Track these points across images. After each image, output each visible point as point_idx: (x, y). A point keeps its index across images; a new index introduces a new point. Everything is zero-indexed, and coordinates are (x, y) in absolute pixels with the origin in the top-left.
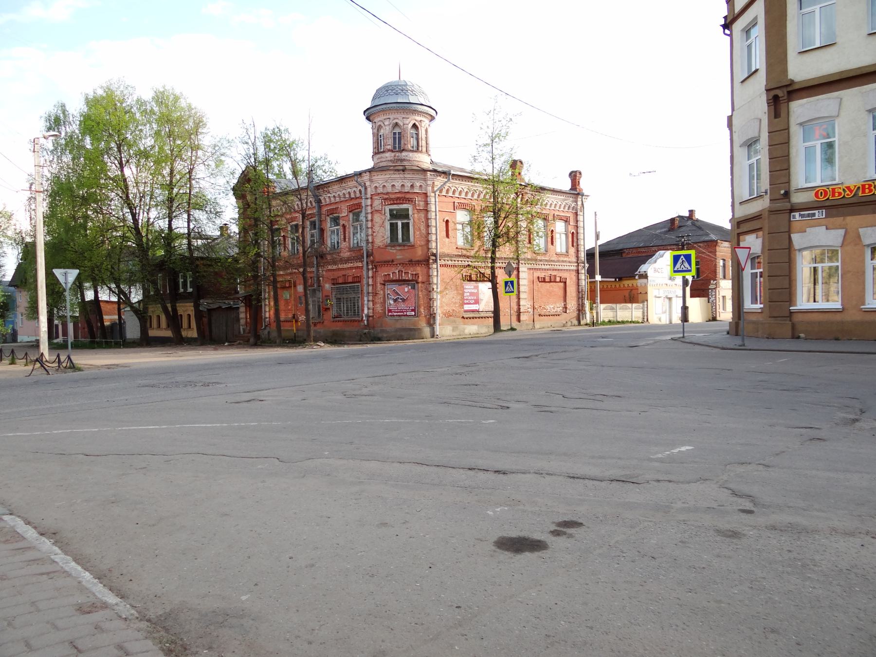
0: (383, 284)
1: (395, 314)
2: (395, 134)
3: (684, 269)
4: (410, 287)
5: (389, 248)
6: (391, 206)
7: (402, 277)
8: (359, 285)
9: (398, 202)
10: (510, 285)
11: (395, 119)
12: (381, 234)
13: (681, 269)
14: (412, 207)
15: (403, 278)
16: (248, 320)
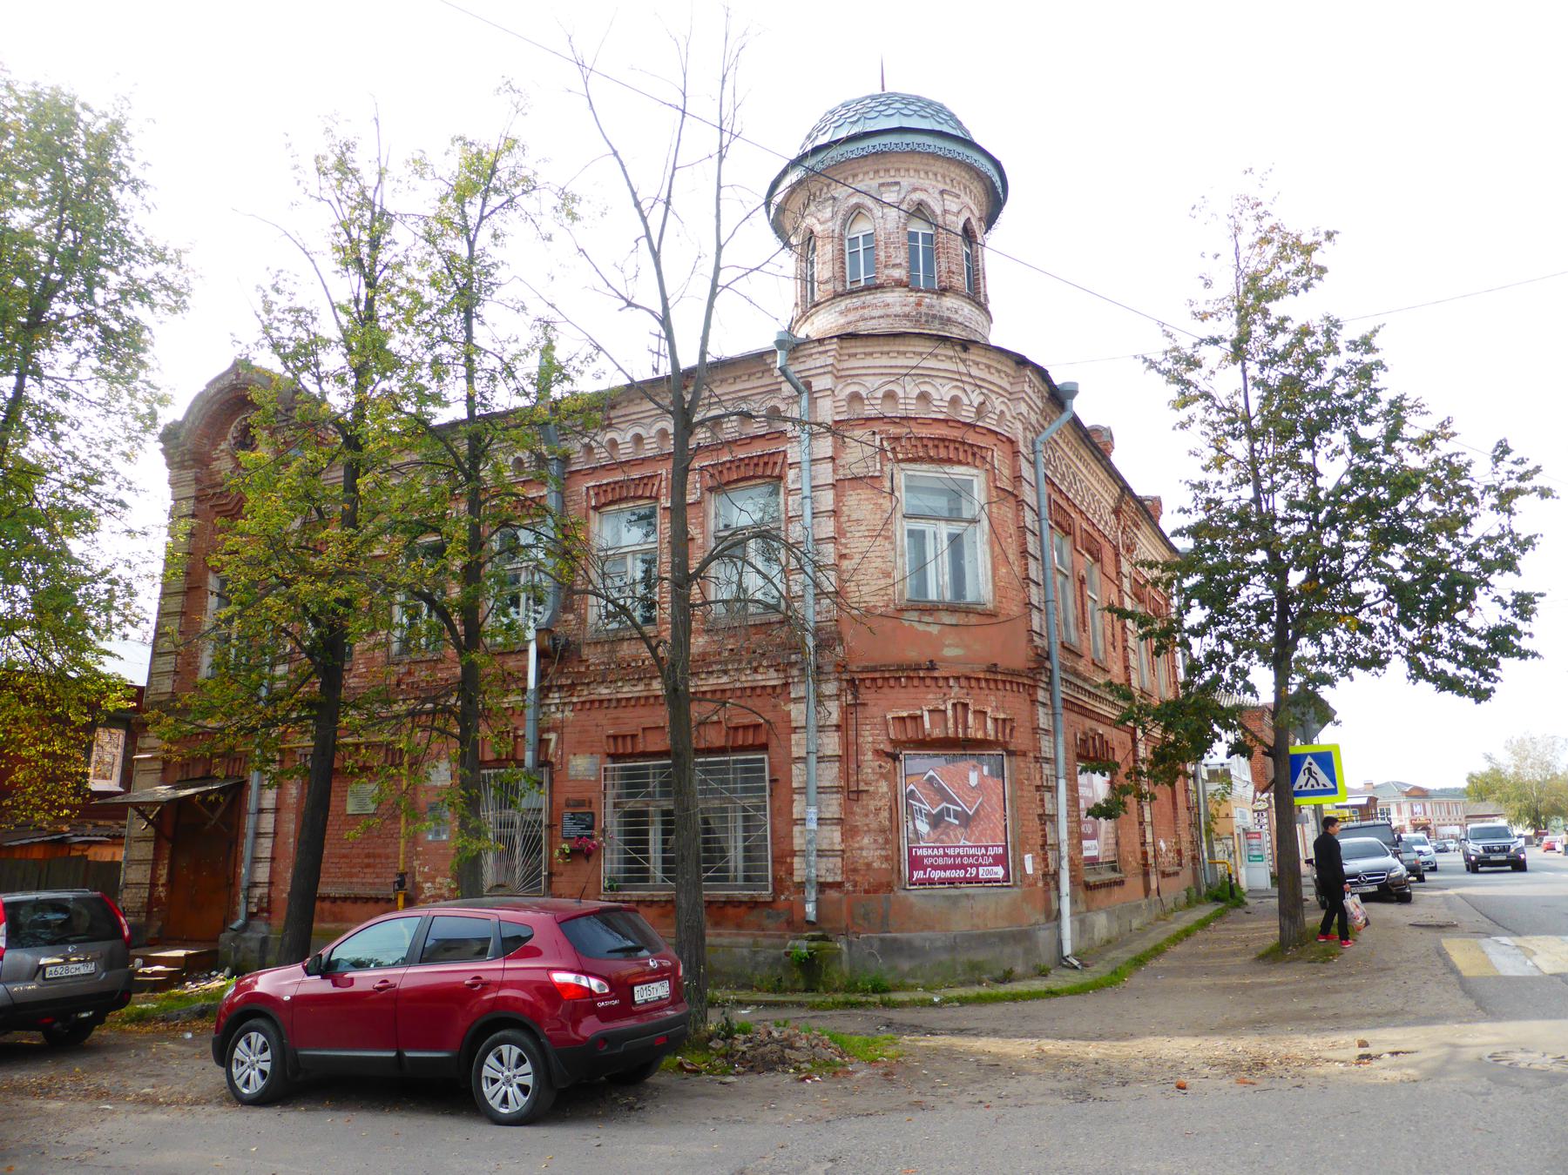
0: (888, 755)
1: (936, 875)
2: (913, 236)
3: (1316, 787)
4: (986, 770)
5: (914, 616)
6: (913, 466)
7: (966, 727)
8: (762, 760)
9: (943, 453)
10: (1315, 768)
11: (915, 190)
12: (878, 563)
13: (1309, 787)
15: (971, 733)
16: (161, 891)
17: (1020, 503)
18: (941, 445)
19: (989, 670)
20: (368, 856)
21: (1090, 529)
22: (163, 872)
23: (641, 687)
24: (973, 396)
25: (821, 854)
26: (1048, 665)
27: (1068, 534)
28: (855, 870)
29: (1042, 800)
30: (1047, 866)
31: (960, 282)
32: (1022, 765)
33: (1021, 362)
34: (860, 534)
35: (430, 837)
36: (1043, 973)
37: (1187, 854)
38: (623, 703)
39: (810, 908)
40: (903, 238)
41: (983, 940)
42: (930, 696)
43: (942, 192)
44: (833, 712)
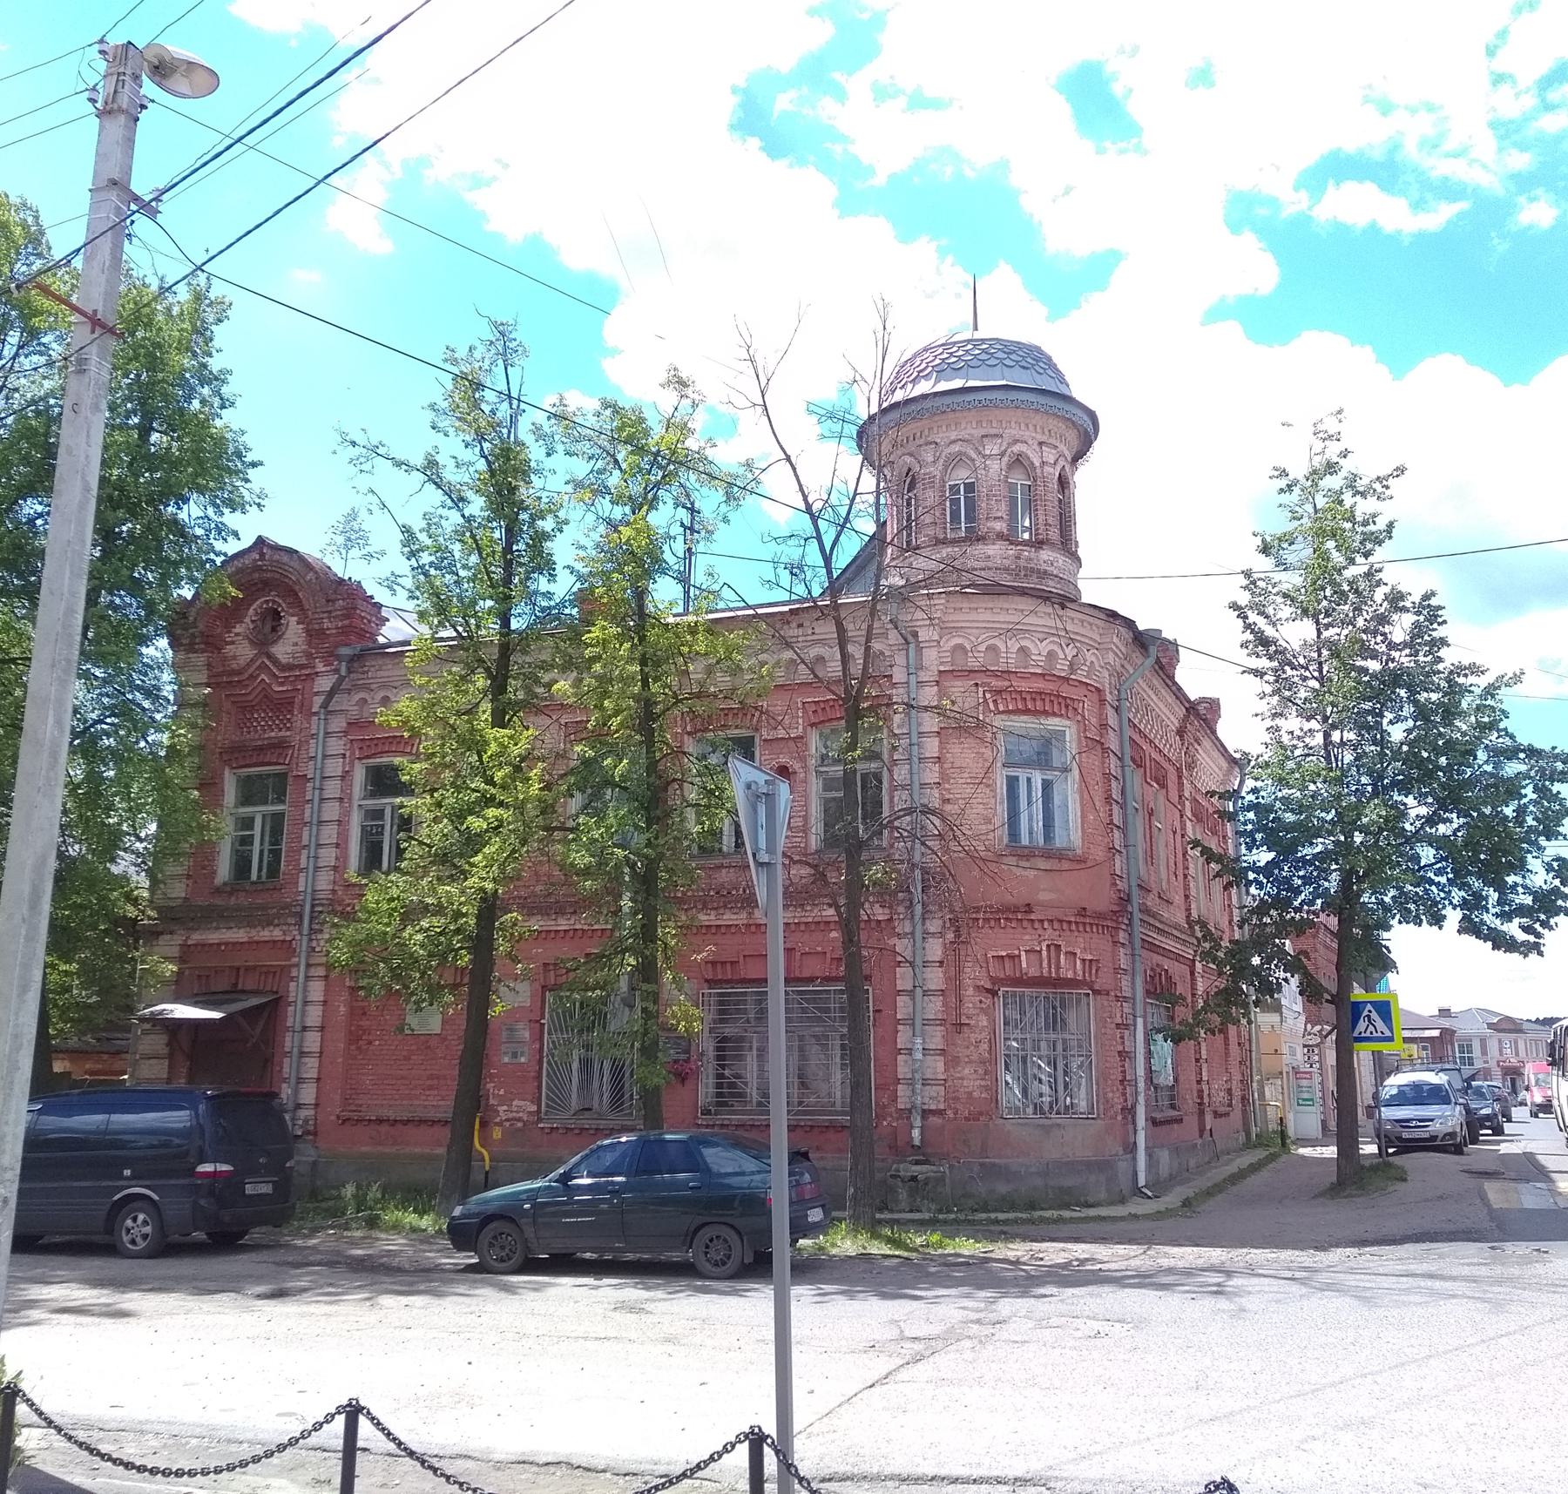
0: (988, 991)
3: (1375, 1034)
7: (1058, 967)
10: (1374, 1015)
11: (1016, 441)
13: (1368, 1034)
14: (1074, 729)
17: (1105, 750)
18: (1038, 697)
19: (1079, 914)
20: (431, 1077)
21: (1158, 758)
23: (744, 915)
24: (1067, 651)
25: (926, 1082)
26: (1130, 909)
27: (1139, 766)
28: (956, 1099)
29: (1122, 1038)
30: (1126, 1101)
31: (1054, 534)
32: (1106, 1003)
33: (1113, 615)
34: (963, 781)
35: (506, 1060)
36: (1122, 1201)
37: (1237, 1093)
38: (723, 930)
39: (916, 1133)
41: (1071, 1166)
42: (1027, 937)
43: (1041, 444)
44: (935, 949)
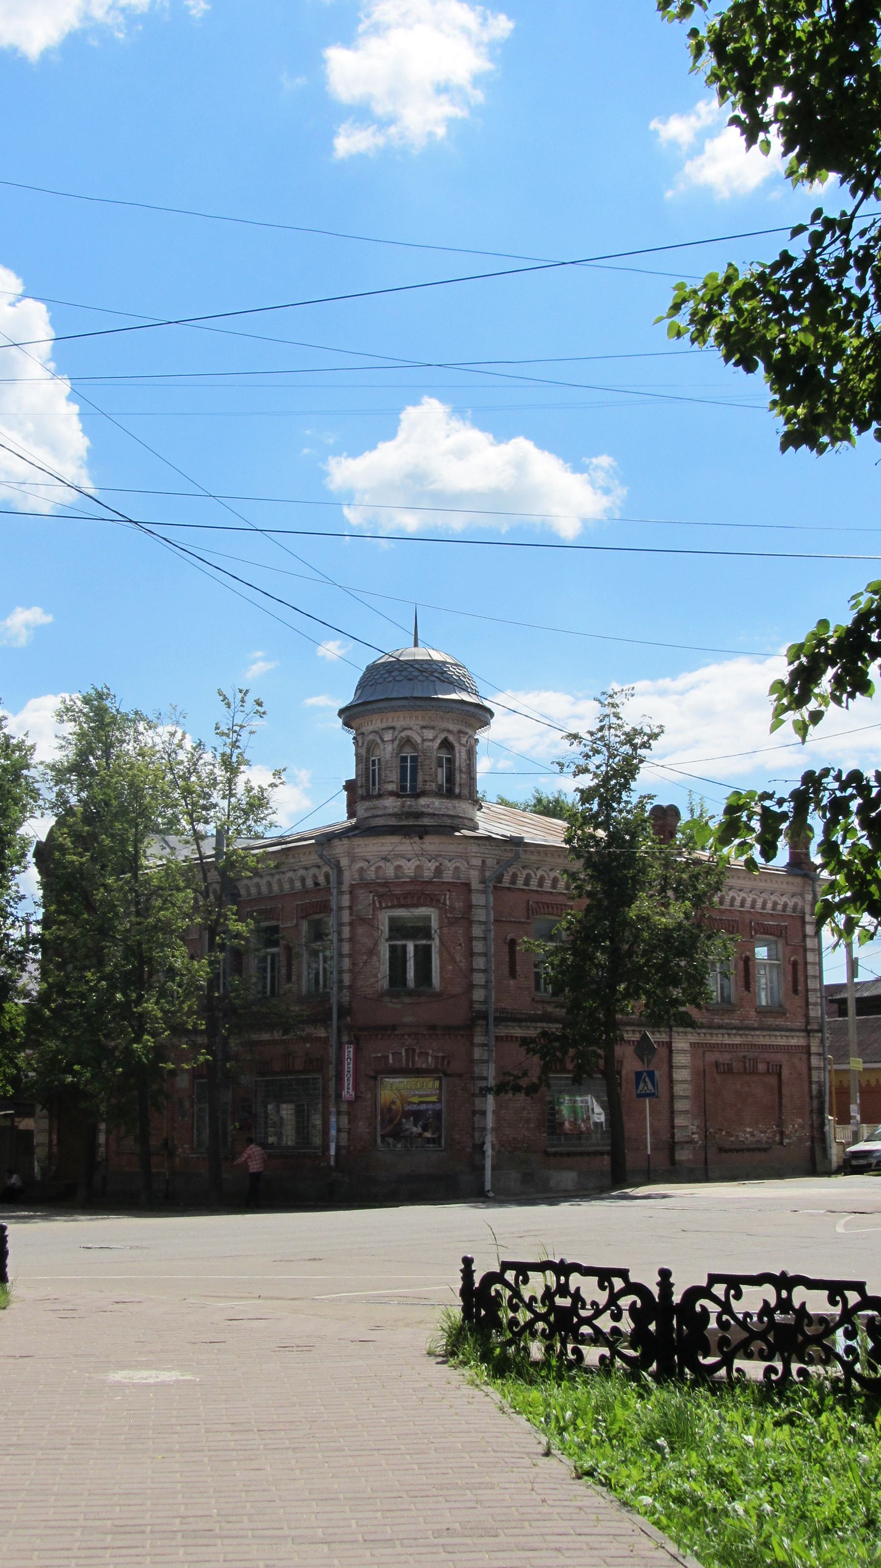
7: (413, 1062)
10: (647, 1079)
11: (404, 729)
16: (55, 1149)
22: (55, 1137)
40: (397, 763)
